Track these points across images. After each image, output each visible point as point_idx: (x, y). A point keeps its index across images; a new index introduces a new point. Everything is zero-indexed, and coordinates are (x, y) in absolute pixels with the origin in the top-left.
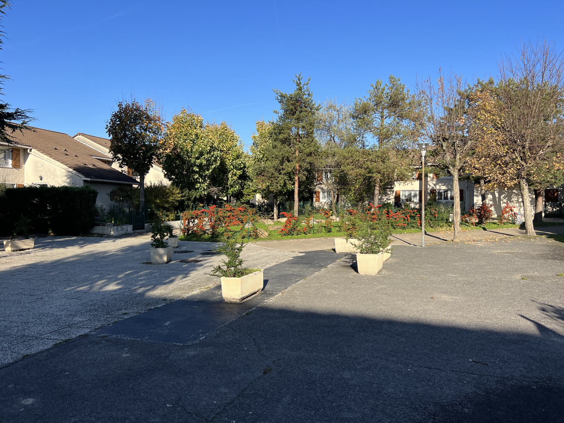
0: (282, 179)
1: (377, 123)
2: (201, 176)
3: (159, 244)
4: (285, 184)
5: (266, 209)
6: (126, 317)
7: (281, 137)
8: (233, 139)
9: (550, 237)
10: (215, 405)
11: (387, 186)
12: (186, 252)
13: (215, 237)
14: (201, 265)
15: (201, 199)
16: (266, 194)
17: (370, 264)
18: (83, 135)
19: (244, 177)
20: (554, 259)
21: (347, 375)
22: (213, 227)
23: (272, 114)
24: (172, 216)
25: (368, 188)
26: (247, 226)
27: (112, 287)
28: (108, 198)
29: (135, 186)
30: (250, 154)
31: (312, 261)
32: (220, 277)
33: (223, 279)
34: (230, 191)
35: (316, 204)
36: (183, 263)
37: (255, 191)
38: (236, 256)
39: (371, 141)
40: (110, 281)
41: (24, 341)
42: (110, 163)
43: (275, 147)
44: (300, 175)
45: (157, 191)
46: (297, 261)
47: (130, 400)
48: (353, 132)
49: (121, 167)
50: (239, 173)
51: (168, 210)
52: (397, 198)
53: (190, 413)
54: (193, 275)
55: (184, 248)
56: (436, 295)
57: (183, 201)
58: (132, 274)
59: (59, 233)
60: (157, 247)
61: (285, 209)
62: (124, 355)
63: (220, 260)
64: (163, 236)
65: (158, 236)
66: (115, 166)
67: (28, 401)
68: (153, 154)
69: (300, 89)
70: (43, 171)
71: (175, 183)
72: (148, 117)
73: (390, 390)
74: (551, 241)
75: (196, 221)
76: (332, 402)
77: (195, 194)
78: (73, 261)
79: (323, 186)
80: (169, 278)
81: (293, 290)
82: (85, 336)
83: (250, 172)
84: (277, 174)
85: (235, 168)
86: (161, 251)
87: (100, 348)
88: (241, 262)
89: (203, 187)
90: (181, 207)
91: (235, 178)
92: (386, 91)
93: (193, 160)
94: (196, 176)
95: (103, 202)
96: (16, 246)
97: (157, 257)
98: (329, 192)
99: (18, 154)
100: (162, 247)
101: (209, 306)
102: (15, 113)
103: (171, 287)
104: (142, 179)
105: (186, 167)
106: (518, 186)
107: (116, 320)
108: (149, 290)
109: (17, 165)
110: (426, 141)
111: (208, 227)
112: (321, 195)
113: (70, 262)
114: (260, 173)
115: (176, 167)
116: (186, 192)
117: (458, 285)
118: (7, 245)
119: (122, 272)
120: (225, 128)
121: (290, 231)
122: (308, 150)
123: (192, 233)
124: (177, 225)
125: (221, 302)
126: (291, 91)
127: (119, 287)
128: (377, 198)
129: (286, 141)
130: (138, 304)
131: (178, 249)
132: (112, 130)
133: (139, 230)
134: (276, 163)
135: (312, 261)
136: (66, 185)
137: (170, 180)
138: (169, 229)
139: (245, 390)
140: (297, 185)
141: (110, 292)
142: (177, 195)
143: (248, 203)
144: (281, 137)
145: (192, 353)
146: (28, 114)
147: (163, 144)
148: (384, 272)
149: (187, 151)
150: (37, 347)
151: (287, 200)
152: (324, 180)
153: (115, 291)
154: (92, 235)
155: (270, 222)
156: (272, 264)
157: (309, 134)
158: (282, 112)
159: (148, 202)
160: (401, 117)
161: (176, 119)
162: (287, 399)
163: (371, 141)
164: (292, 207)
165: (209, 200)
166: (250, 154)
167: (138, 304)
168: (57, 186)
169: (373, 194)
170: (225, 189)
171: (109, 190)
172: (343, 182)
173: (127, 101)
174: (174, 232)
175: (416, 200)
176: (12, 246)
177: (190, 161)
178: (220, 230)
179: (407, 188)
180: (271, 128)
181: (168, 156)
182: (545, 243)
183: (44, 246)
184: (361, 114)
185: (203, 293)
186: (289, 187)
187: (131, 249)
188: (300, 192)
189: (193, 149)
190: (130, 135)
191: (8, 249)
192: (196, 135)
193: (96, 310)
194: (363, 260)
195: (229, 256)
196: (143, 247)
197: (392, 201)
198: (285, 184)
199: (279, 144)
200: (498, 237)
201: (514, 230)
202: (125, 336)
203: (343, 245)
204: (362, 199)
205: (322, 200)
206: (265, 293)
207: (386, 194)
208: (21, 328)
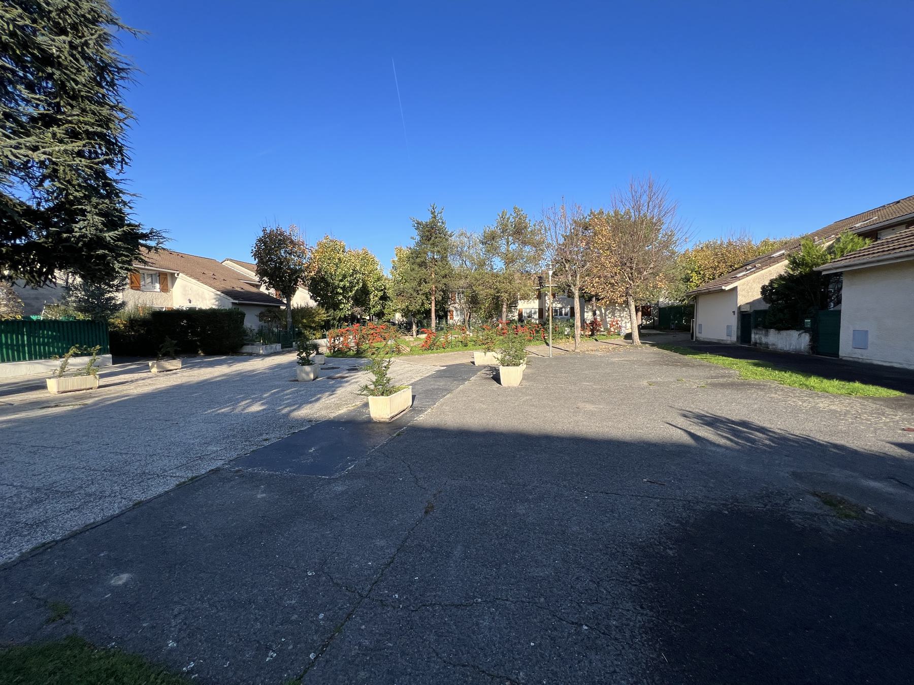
0: (420, 298)
1: (503, 249)
2: (345, 297)
3: (305, 362)
4: (423, 304)
5: (406, 327)
6: (266, 444)
7: (418, 260)
8: (374, 263)
9: (653, 345)
10: (371, 568)
11: (512, 304)
12: (333, 368)
13: (359, 354)
14: (347, 382)
15: (345, 319)
16: (406, 313)
17: (511, 376)
18: (231, 260)
19: (384, 298)
20: (668, 365)
21: (521, 509)
22: (358, 344)
23: (409, 240)
24: (318, 335)
25: (496, 306)
26: (389, 343)
27: (256, 408)
28: (257, 319)
29: (283, 307)
30: (390, 277)
31: (456, 374)
32: (367, 396)
33: (371, 398)
34: (372, 311)
35: (450, 322)
36: (329, 380)
37: (395, 311)
38: (383, 375)
39: (498, 264)
40: (255, 401)
41: (142, 481)
42: (258, 286)
43: (412, 270)
44: (437, 295)
45: (304, 312)
46: (440, 375)
47: (261, 566)
48: (482, 256)
49: (267, 289)
50: (380, 294)
51: (314, 329)
52: (520, 315)
53: (338, 584)
54: (340, 391)
55: (331, 365)
56: (581, 405)
57: (329, 321)
58: (278, 392)
59: (209, 353)
60: (303, 364)
61: (423, 326)
62: (259, 496)
63: (365, 378)
64: (308, 354)
65: (304, 354)
66: (263, 289)
67: (120, 579)
68: (298, 277)
69: (435, 217)
70: (191, 294)
71: (321, 304)
72: (292, 242)
73: (576, 528)
74: (655, 349)
75: (342, 339)
76: (514, 552)
77: (340, 314)
78: (219, 381)
79: (456, 305)
80: (315, 395)
81: (442, 405)
82: (217, 470)
83: (390, 293)
84: (415, 294)
85: (377, 289)
86: (307, 368)
87: (231, 487)
88: (389, 380)
89: (347, 308)
90: (327, 325)
91: (377, 299)
92: (511, 219)
93: (337, 283)
94: (340, 297)
95: (251, 322)
96: (163, 367)
97: (304, 375)
98: (462, 310)
99: (165, 279)
100: (309, 364)
101: (356, 427)
102: (151, 233)
103: (317, 405)
104: (289, 300)
105: (330, 289)
106: (627, 303)
107: (255, 448)
108: (294, 410)
109: (165, 289)
110: (545, 265)
111: (353, 344)
112: (455, 313)
113: (216, 382)
114: (400, 294)
115: (321, 290)
116: (331, 312)
117: (597, 394)
118: (153, 366)
119: (268, 391)
120: (366, 253)
121: (429, 347)
122: (443, 273)
123: (338, 350)
124: (324, 344)
125: (370, 421)
126: (426, 218)
127: (261, 408)
128: (504, 315)
129: (423, 264)
130: (281, 427)
131: (325, 366)
132: (257, 255)
133: (287, 347)
134: (415, 284)
135: (456, 374)
136: (214, 307)
137: (316, 301)
138: (316, 347)
139: (405, 541)
140: (433, 304)
141: (252, 413)
142: (323, 315)
143: (389, 321)
144: (418, 260)
145: (339, 488)
146: (164, 235)
147: (308, 267)
148: (525, 383)
149: (331, 274)
150: (158, 488)
151: (425, 318)
152: (457, 301)
153: (258, 412)
154: (242, 354)
155: (411, 339)
156: (417, 379)
157: (444, 258)
158: (418, 238)
159: (295, 322)
160: (524, 243)
161: (319, 244)
162: (458, 552)
163: (498, 264)
164: (429, 325)
165: (353, 319)
166: (390, 277)
167: (281, 427)
168: (204, 308)
169: (501, 311)
170: (367, 310)
171: (257, 311)
172: (474, 301)
173: (271, 227)
174: (320, 350)
175: (536, 316)
176: (158, 367)
177: (333, 284)
178: (364, 346)
179: (529, 306)
180: (408, 252)
181: (313, 279)
182: (650, 352)
183: (192, 366)
184: (490, 240)
185: (351, 411)
186: (427, 306)
187: (280, 366)
188: (436, 311)
189: (336, 273)
190: (276, 260)
191: (154, 370)
192: (339, 259)
193: (234, 436)
194: (504, 371)
195: (375, 374)
196: (290, 365)
197: (516, 318)
198: (423, 304)
199: (416, 267)
200: (611, 347)
201: (620, 340)
202: (262, 469)
203: (483, 358)
204: (491, 316)
205: (456, 318)
206: (414, 410)
207: (511, 312)
208: (143, 463)
